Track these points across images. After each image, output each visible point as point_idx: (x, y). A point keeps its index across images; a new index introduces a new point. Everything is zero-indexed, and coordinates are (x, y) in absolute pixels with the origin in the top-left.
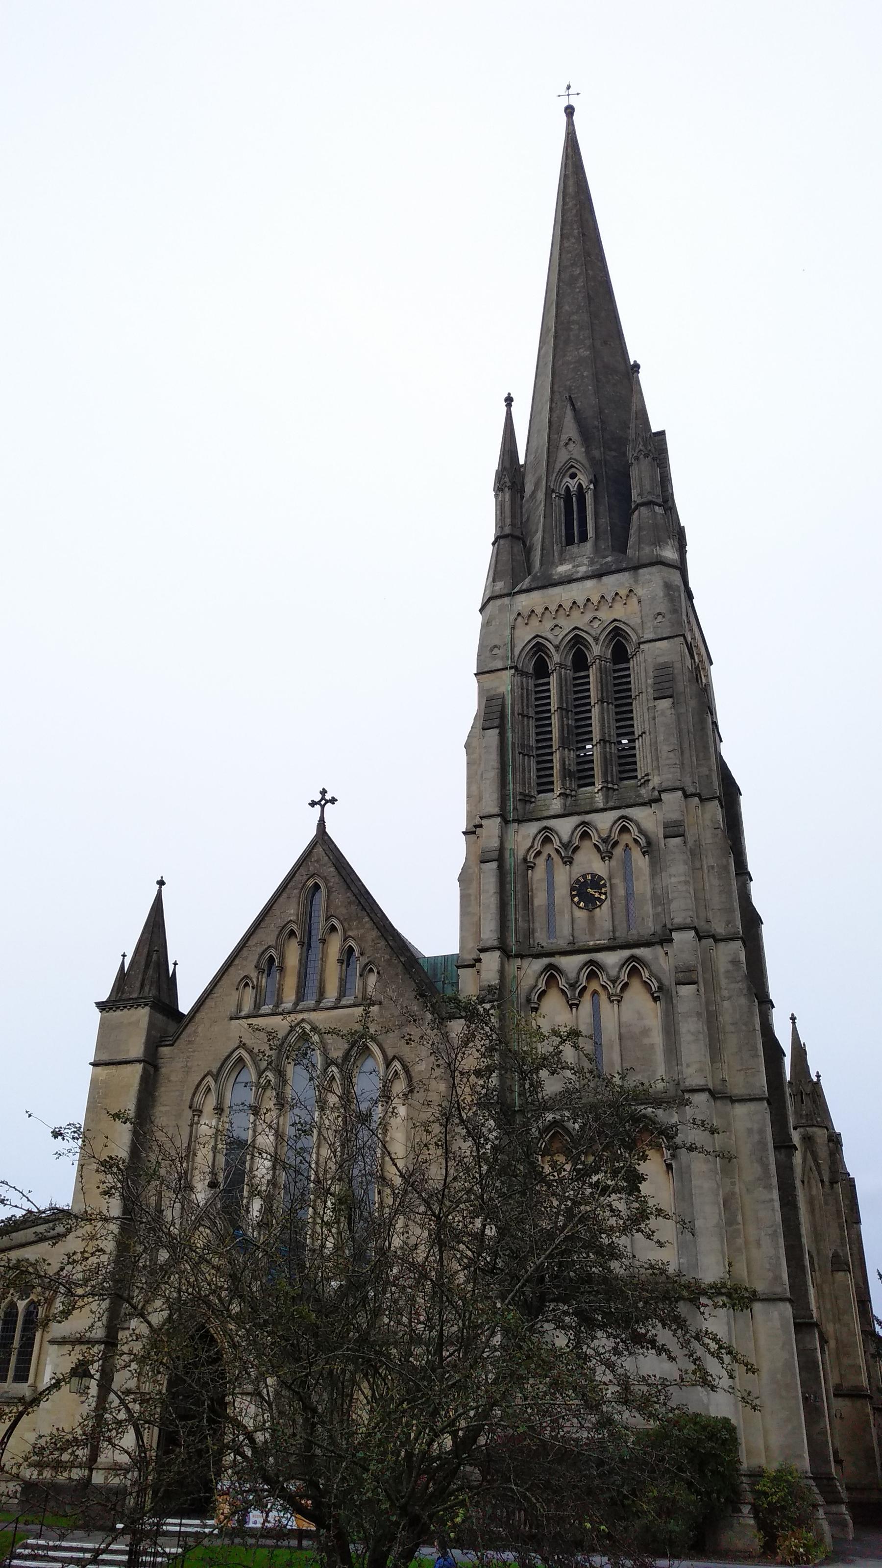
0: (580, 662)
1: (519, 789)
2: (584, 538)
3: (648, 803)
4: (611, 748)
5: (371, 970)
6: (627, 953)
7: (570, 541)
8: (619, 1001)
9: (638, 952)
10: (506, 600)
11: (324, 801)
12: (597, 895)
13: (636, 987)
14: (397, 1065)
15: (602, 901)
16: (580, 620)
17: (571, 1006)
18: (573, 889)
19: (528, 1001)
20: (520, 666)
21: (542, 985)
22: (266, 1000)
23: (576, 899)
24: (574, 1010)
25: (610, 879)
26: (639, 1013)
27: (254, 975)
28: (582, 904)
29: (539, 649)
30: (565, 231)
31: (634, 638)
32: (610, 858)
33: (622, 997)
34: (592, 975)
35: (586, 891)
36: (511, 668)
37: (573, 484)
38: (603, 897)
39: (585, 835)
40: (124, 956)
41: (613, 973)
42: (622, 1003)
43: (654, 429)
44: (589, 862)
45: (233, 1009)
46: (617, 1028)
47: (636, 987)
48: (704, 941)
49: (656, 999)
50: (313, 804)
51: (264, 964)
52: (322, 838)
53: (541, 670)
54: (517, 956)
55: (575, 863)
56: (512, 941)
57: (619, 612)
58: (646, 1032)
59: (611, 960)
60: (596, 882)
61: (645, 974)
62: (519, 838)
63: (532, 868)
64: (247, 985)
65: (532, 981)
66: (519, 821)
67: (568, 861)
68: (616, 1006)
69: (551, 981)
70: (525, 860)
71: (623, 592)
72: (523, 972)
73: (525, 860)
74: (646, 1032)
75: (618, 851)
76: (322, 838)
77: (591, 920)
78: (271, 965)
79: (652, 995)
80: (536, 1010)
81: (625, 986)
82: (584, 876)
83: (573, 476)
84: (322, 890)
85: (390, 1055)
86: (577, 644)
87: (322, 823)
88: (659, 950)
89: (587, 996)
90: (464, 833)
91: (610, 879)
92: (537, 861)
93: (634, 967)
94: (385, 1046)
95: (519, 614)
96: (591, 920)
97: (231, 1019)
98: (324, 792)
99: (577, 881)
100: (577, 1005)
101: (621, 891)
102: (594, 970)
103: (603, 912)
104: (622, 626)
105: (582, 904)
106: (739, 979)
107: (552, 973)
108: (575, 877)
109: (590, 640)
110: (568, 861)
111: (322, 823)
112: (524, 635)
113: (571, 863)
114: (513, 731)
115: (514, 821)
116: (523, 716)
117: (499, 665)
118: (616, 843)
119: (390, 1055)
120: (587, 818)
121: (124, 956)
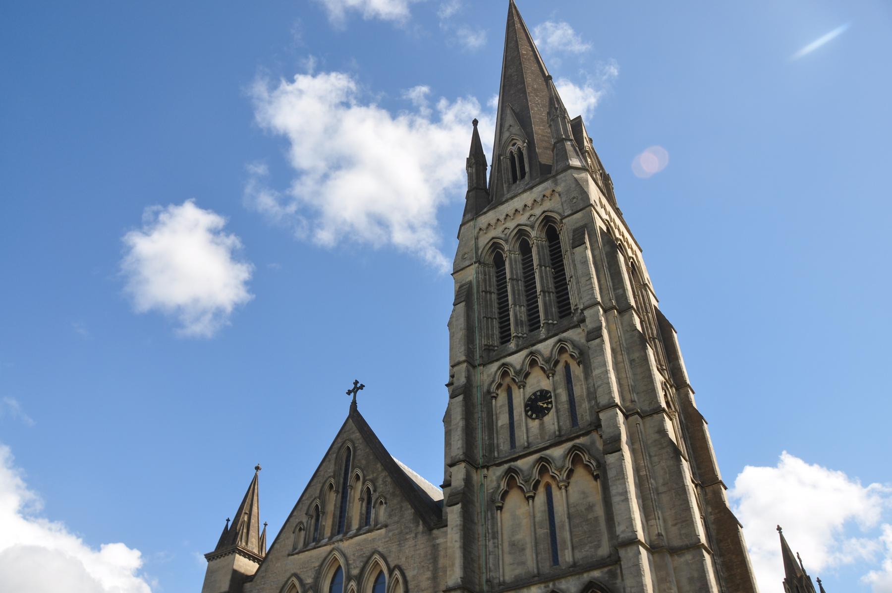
0: (525, 249)
1: (484, 342)
2: (523, 174)
3: (577, 326)
4: (549, 296)
5: (381, 503)
6: (569, 445)
7: (515, 180)
8: (566, 487)
9: (577, 441)
10: (471, 223)
11: (357, 387)
12: (545, 405)
13: (580, 472)
14: (397, 572)
15: (549, 409)
16: (523, 219)
17: (528, 499)
18: (526, 406)
19: (493, 501)
20: (482, 260)
21: (503, 486)
22: (314, 540)
23: (529, 413)
24: (531, 501)
25: (554, 390)
26: (584, 493)
27: (305, 520)
28: (534, 416)
29: (495, 247)
30: (643, 473)
31: (558, 217)
32: (553, 375)
33: (569, 483)
34: (543, 471)
35: (537, 406)
36: (475, 263)
37: (514, 149)
38: (550, 406)
39: (533, 363)
40: (228, 520)
41: (559, 464)
42: (569, 488)
43: (572, 116)
44: (538, 381)
45: (290, 548)
46: (566, 509)
47: (580, 472)
48: (630, 418)
49: (596, 478)
50: (349, 393)
51: (312, 511)
52: (354, 414)
53: (499, 262)
54: (483, 467)
55: (528, 386)
56: (479, 455)
57: (547, 205)
58: (590, 508)
59: (557, 452)
60: (543, 395)
61: (586, 458)
62: (485, 377)
63: (496, 398)
64: (300, 529)
65: (494, 484)
66: (484, 365)
67: (522, 386)
68: (564, 491)
69: (511, 483)
70: (489, 392)
71: (548, 193)
72: (489, 479)
73: (489, 392)
74: (590, 508)
75: (560, 367)
76: (354, 414)
77: (542, 425)
78: (318, 513)
79: (593, 474)
80: (500, 508)
81: (571, 472)
82: (534, 394)
83: (514, 145)
84: (357, 454)
85: (392, 565)
86: (521, 234)
87: (354, 404)
88: (595, 435)
89: (541, 489)
90: (447, 385)
91: (554, 390)
92: (499, 392)
93: (575, 456)
94: (389, 560)
95: (480, 229)
96: (542, 425)
97: (289, 555)
98: (356, 383)
99: (530, 399)
100: (533, 498)
101: (564, 397)
102: (544, 465)
103: (550, 419)
104: (549, 214)
105: (534, 416)
106: (664, 445)
107: (511, 475)
108: (527, 397)
109: (528, 229)
110: (522, 386)
111: (354, 404)
112: (484, 240)
113: (524, 386)
114: (479, 304)
115: (479, 365)
116: (486, 292)
117: (467, 263)
118: (557, 363)
119: (392, 565)
120: (534, 348)
121: (228, 520)
